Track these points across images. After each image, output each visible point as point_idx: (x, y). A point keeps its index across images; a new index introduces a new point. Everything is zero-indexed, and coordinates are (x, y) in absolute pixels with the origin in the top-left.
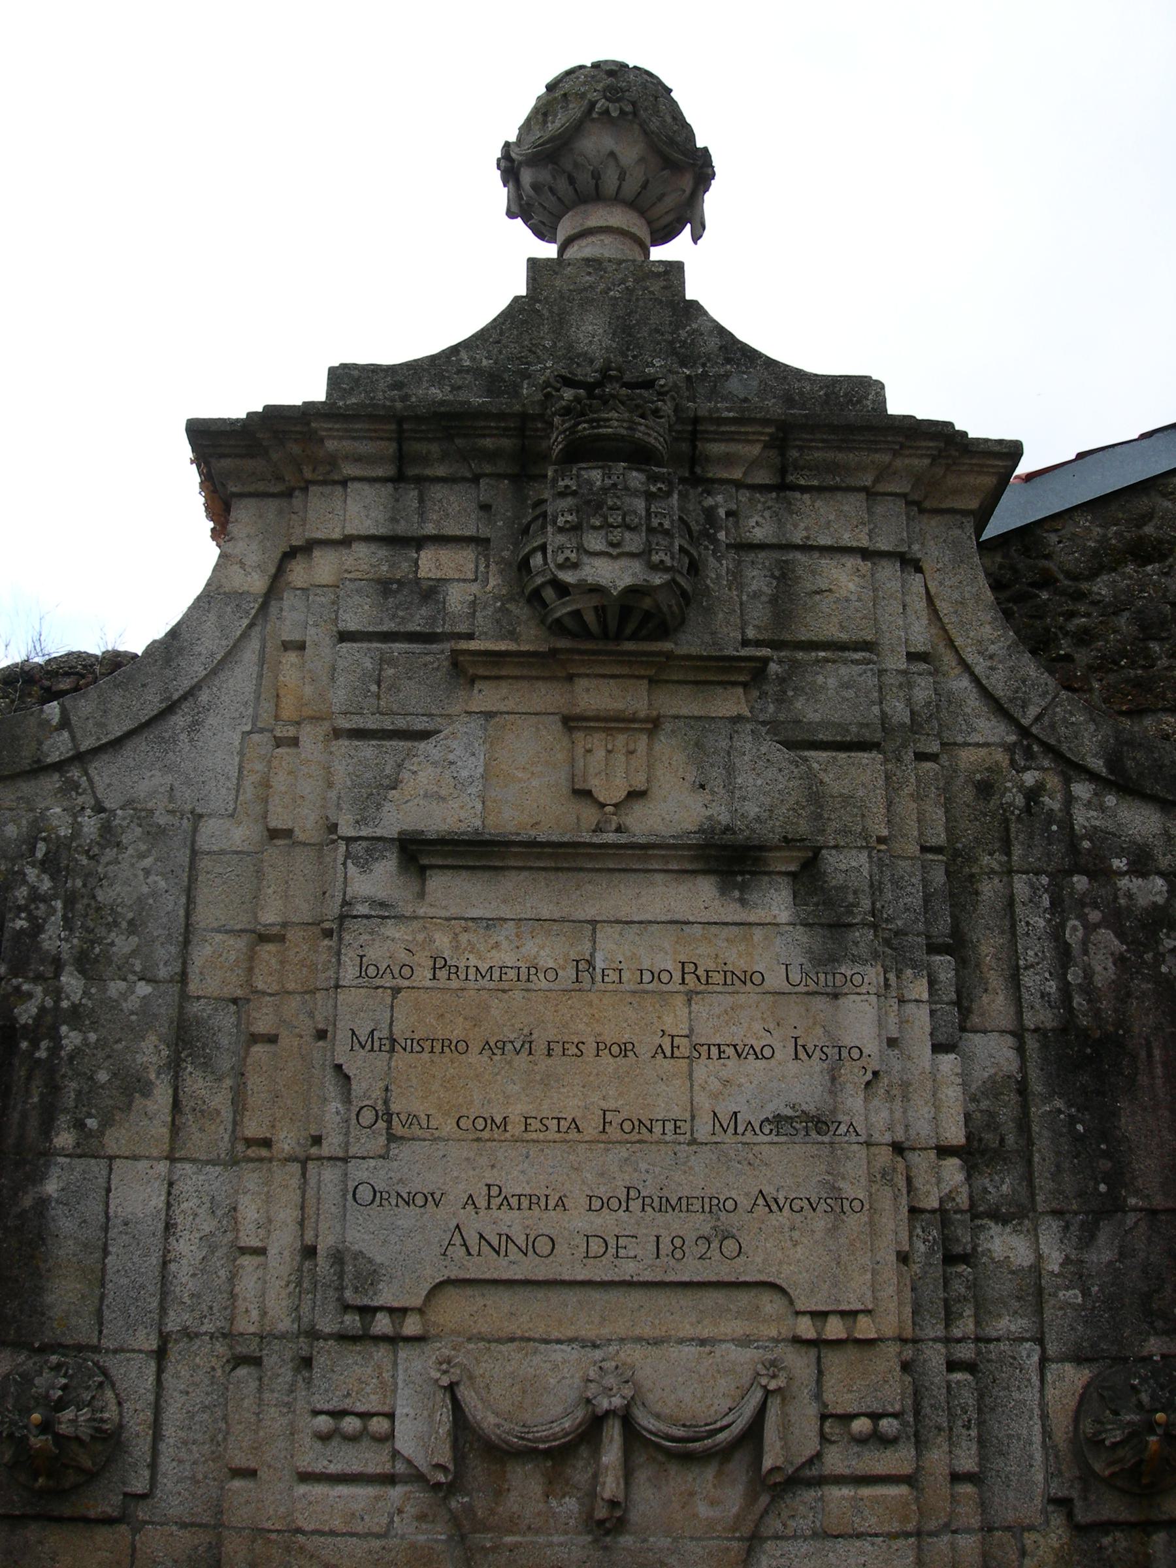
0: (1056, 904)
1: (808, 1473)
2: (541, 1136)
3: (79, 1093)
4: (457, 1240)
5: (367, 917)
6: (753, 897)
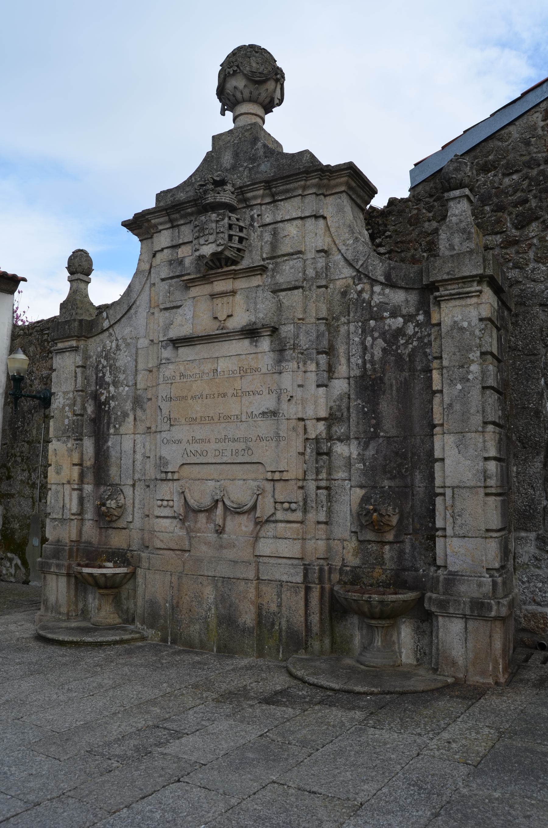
0: (363, 331)
1: (272, 519)
2: (204, 422)
3: (115, 418)
4: (185, 453)
5: (165, 363)
6: (259, 344)
